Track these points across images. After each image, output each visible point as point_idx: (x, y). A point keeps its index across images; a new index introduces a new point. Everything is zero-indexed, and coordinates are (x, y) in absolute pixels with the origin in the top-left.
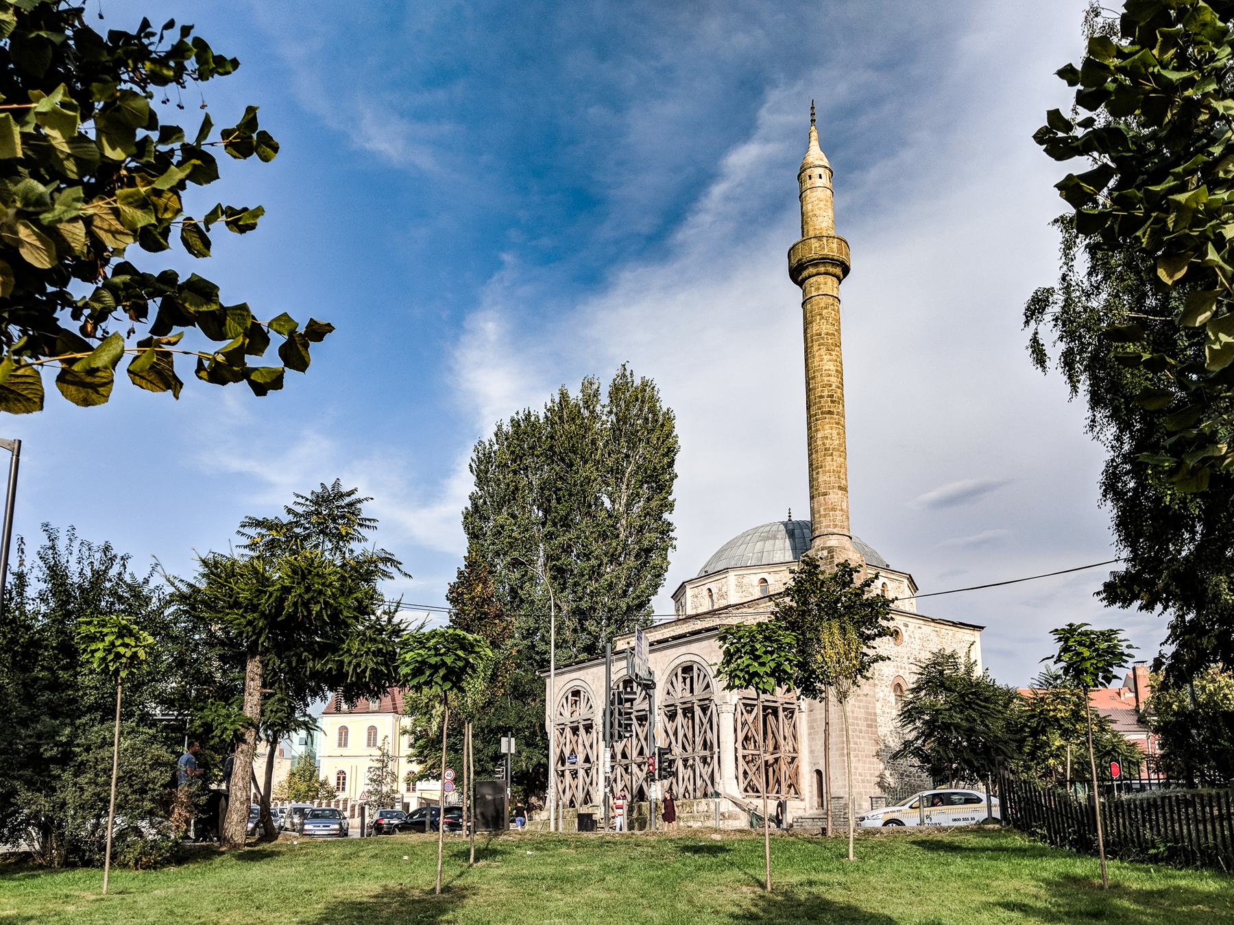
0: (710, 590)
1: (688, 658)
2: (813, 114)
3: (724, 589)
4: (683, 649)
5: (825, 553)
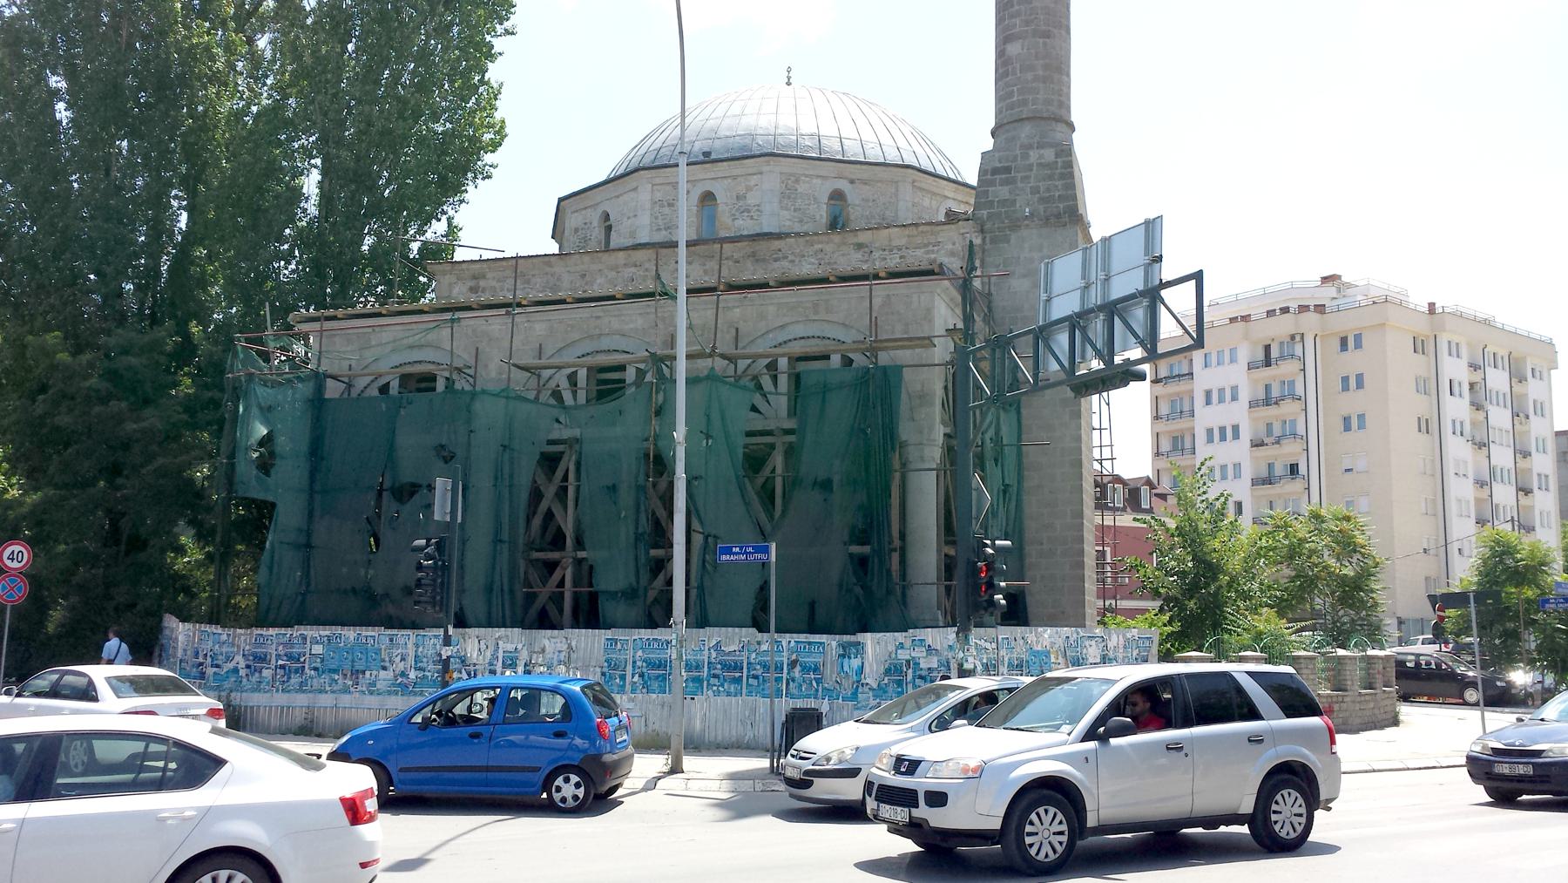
0: (708, 198)
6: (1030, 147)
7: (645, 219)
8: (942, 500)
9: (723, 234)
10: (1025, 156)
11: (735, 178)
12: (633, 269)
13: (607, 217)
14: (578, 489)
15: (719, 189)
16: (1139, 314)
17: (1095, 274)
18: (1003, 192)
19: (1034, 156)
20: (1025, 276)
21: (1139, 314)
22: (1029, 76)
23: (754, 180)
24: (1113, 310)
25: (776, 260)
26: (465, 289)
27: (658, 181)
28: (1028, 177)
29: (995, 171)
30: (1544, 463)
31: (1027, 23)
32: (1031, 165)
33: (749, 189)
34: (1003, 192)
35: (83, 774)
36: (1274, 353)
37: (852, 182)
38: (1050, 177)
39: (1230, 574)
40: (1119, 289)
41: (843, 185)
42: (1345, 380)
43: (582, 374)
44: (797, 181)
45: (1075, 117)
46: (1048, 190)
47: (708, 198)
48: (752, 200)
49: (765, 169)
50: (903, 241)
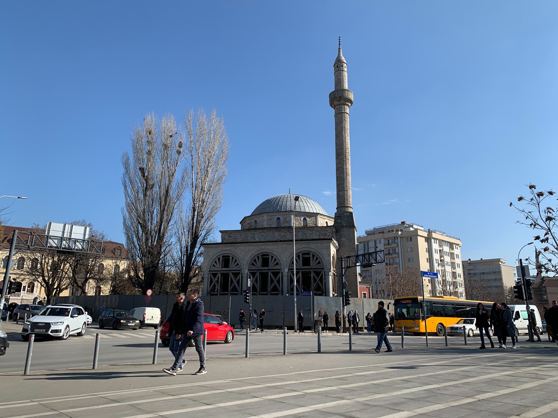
0: (278, 219)
3: (288, 219)
7: (265, 223)
8: (539, 353)
9: (282, 226)
13: (256, 221)
15: (281, 217)
16: (374, 255)
17: (366, 247)
18: (340, 221)
21: (374, 255)
24: (370, 254)
29: (338, 217)
30: (459, 271)
34: (340, 221)
36: (390, 242)
39: (56, 237)
40: (370, 251)
42: (409, 259)
43: (221, 258)
47: (278, 219)
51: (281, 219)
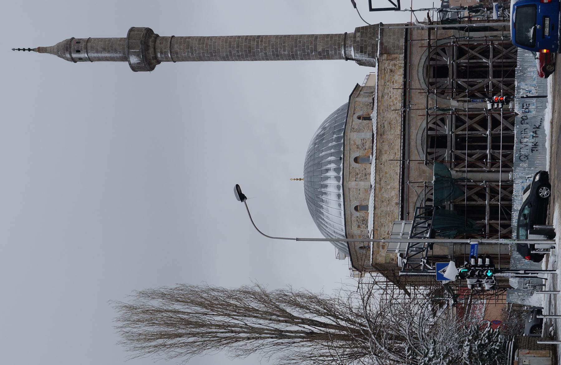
0: (356, 160)
1: (419, 142)
2: (24, 50)
3: (359, 142)
4: (413, 143)
5: (358, 34)
6: (355, 41)
10: (358, 42)
11: (350, 149)
12: (382, 182)
14: (491, 244)
15: (354, 155)
19: (358, 39)
20: (399, 41)
22: (330, 42)
23: (352, 142)
25: (384, 127)
26: (383, 251)
27: (348, 179)
28: (365, 41)
31: (311, 43)
32: (361, 40)
33: (355, 144)
35: (545, 340)
37: (354, 113)
38: (366, 33)
41: (355, 116)
44: (353, 128)
45: (85, 36)
46: (370, 34)
48: (359, 142)
49: (348, 138)
50: (383, 81)
51: (357, 154)
